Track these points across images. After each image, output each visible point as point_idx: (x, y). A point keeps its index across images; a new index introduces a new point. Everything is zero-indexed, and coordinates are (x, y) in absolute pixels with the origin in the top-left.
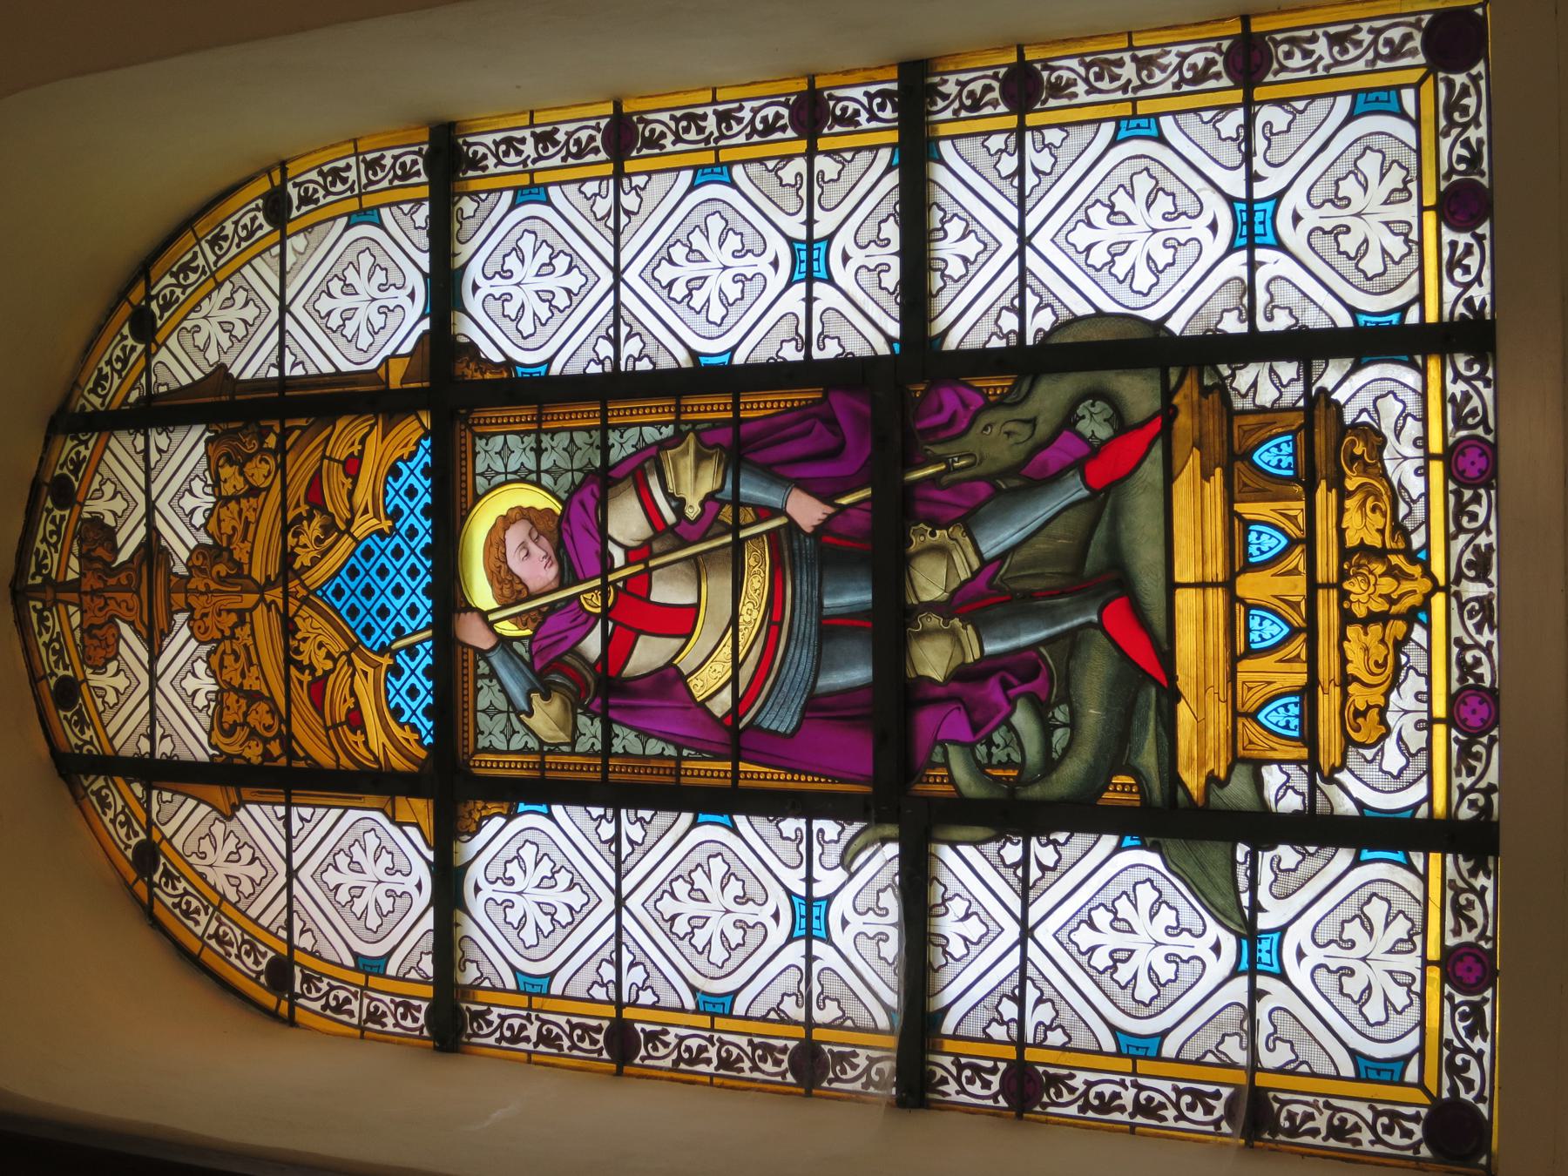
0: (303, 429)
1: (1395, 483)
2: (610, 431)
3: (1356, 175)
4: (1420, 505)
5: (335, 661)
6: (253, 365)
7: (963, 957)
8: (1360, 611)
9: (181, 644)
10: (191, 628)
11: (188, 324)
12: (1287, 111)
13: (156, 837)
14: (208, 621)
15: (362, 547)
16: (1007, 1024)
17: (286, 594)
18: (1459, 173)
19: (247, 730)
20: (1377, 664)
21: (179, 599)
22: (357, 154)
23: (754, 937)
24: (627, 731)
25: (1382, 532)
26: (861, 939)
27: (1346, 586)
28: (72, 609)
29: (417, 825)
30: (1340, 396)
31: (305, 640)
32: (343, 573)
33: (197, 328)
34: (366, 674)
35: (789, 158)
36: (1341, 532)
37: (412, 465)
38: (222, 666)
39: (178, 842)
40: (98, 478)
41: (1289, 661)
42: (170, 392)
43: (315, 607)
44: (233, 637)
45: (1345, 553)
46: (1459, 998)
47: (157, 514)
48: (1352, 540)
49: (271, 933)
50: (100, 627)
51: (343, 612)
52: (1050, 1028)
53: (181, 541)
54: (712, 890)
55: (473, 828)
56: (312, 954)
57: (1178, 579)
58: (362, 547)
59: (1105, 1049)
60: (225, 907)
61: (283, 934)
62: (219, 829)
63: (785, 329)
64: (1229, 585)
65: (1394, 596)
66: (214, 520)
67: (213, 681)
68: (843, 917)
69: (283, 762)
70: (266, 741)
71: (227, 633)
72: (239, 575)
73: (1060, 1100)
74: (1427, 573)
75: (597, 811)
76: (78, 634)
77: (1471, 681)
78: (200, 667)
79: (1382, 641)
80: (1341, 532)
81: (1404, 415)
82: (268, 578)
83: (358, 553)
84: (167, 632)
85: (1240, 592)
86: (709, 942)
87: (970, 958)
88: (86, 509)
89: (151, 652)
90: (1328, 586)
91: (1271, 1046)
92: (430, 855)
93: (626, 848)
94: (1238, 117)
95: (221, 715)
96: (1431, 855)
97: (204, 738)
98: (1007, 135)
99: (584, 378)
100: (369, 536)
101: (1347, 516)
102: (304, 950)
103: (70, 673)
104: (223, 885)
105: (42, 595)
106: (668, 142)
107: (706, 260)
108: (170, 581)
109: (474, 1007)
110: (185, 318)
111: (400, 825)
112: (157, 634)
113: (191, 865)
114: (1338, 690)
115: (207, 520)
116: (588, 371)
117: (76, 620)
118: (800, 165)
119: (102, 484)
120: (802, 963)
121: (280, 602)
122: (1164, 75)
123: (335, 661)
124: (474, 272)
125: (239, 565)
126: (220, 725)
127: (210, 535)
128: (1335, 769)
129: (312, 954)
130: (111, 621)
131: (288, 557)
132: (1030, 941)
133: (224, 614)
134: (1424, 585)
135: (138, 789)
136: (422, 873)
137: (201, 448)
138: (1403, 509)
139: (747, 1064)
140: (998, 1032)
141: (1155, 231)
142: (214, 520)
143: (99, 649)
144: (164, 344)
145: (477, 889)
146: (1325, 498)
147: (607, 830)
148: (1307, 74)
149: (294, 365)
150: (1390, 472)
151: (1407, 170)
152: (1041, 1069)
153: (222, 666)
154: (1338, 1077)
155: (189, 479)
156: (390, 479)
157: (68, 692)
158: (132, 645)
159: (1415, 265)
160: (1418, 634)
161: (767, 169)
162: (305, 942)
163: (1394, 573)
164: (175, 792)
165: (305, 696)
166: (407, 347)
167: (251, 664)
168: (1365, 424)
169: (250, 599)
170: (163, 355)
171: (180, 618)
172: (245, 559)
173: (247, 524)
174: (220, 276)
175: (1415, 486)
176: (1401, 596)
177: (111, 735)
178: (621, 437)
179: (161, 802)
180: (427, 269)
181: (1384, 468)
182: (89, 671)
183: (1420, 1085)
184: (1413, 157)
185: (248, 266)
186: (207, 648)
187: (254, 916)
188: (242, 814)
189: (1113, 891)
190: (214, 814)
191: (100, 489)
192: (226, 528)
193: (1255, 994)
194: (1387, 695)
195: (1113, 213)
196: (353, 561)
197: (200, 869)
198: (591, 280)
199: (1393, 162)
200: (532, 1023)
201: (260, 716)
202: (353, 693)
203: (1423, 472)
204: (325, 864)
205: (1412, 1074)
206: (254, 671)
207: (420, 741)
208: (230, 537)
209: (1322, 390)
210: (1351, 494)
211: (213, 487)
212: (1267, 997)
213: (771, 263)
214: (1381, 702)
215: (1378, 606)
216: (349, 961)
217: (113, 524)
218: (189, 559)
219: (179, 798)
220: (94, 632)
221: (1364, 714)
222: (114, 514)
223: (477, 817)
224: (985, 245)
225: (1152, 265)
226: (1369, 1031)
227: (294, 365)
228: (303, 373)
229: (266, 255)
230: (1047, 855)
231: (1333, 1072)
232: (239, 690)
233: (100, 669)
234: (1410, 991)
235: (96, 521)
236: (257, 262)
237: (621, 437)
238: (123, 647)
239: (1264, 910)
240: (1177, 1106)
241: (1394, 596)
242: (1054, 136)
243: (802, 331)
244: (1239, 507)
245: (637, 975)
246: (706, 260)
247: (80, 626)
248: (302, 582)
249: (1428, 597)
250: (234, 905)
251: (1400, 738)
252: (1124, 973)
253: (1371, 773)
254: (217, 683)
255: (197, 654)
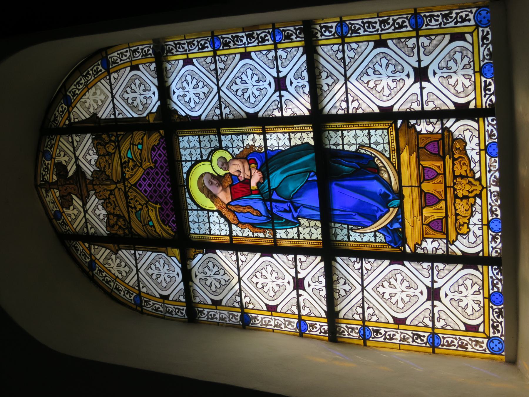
0: (124, 135)
1: (470, 157)
2: (267, 135)
3: (453, 60)
4: (478, 164)
5: (142, 206)
6: (105, 113)
7: (344, 296)
8: (460, 195)
9: (93, 201)
10: (95, 195)
11: (83, 100)
12: (285, 52)
13: (94, 258)
14: (101, 193)
15: (146, 172)
16: (359, 314)
17: (125, 186)
18: (487, 59)
19: (118, 227)
20: (466, 210)
21: (90, 187)
22: (129, 47)
23: (282, 289)
24: (381, 235)
25: (466, 171)
26: (314, 289)
27: (455, 187)
28: (56, 191)
29: (175, 257)
30: (452, 129)
31: (132, 199)
32: (141, 180)
33: (85, 102)
34: (152, 210)
35: (410, 38)
36: (454, 171)
37: (158, 147)
38: (107, 207)
39: (101, 260)
40: (58, 150)
41: (438, 209)
42: (79, 122)
43: (133, 189)
44: (109, 198)
45: (455, 177)
46: (495, 307)
47: (79, 161)
48: (457, 173)
49: (133, 287)
50: (66, 196)
51: (143, 191)
52: (249, 303)
53: (89, 169)
54: (398, 285)
55: (192, 257)
56: (146, 293)
57: (403, 185)
58: (146, 172)
59: (461, 329)
60: (117, 279)
61: (137, 288)
62: (113, 257)
63: (414, 97)
64: (419, 186)
65: (470, 191)
66: (98, 163)
67: (105, 211)
68: (446, 293)
69: (130, 236)
70: (124, 229)
71: (108, 197)
72: (109, 179)
73: (377, 336)
74: (481, 184)
75: (231, 252)
76: (59, 198)
77: (495, 217)
78: (100, 207)
79: (467, 204)
80: (454, 171)
81: (473, 136)
82: (118, 180)
83: (145, 173)
84: (88, 197)
85: (423, 188)
86: (162, 281)
87: (347, 296)
88: (56, 160)
89: (83, 202)
90: (450, 187)
91: (439, 321)
92: (180, 265)
93: (365, 271)
94: (273, 53)
95: (109, 222)
96: (484, 266)
97: (105, 229)
98: (339, 45)
99: (214, 121)
100: (148, 168)
101: (455, 166)
102: (144, 292)
103: (58, 209)
104: (117, 274)
105: (45, 186)
106: (361, 31)
107: (247, 83)
108: (86, 181)
109: (200, 309)
110: (81, 98)
111: (170, 257)
112: (84, 197)
113: (106, 268)
114: (454, 217)
115: (96, 163)
116: (338, 113)
117: (58, 194)
118: (414, 40)
119: (60, 152)
120: (431, 308)
121: (123, 188)
122: (451, 20)
123: (142, 206)
124: (173, 87)
125: (108, 176)
126: (108, 225)
127: (98, 168)
128: (454, 241)
129: (146, 293)
130: (69, 194)
131: (123, 173)
132: (365, 291)
133: (106, 191)
134: (480, 188)
135: (87, 245)
136: (178, 270)
137: (90, 140)
138: (473, 165)
139: (174, 313)
140: (357, 317)
141: (254, 86)
142: (98, 163)
143: (66, 202)
144: (75, 106)
145: (196, 276)
146: (448, 161)
147: (358, 266)
148: (438, 26)
149: (119, 114)
150: (468, 154)
151: (470, 58)
152: (250, 315)
153: (107, 207)
154: (389, 323)
155: (88, 149)
156: (152, 152)
157: (58, 215)
158: (77, 202)
159: (473, 88)
160: (478, 201)
161: (401, 42)
162: (144, 290)
163: (470, 183)
164: (98, 246)
165: (134, 216)
166: (154, 110)
167: (116, 206)
168: (460, 138)
169: (113, 186)
170: (75, 109)
171: (92, 193)
172: (110, 174)
173: (109, 164)
174: (89, 86)
175: (477, 158)
176: (472, 191)
177: (75, 228)
178: (271, 136)
179: (94, 249)
180: (157, 84)
181: (466, 152)
182: (64, 209)
183: (484, 332)
184: (472, 55)
185: (99, 82)
186: (102, 201)
187: (127, 282)
188: (120, 252)
189: (389, 276)
190: (112, 252)
191: (59, 154)
192: (102, 165)
193: (299, 295)
194: (469, 220)
195: (375, 71)
196: (144, 176)
197: (109, 269)
198: (211, 90)
199: (465, 56)
200: (272, 320)
201: (121, 223)
202: (149, 216)
203: (479, 154)
204: (378, 285)
205: (481, 329)
206: (118, 208)
207: (172, 230)
208: (104, 168)
209: (446, 127)
210: (457, 159)
211: (96, 152)
212: (436, 307)
213: (293, 83)
214: (467, 222)
215: (466, 194)
216: (158, 296)
217: (65, 164)
218: (92, 175)
219: (100, 248)
220: (64, 197)
221: (463, 225)
222: (65, 161)
223: (193, 254)
224: (360, 79)
225: (389, 87)
226: (469, 317)
227: (119, 114)
228: (122, 117)
229: (105, 79)
230: (368, 266)
231: (459, 329)
232: (114, 215)
233: (68, 208)
234: (479, 306)
235: (60, 163)
236: (102, 81)
237: (271, 136)
238: (74, 202)
239: (300, 273)
240: (229, 318)
241: (470, 191)
242: (354, 46)
243: (419, 99)
244: (421, 162)
245: (370, 311)
246: (247, 83)
247: (59, 196)
248: (129, 182)
249: (481, 191)
250: (120, 279)
251: (473, 232)
252: (266, 289)
253: (465, 242)
254: (106, 212)
255: (98, 203)
